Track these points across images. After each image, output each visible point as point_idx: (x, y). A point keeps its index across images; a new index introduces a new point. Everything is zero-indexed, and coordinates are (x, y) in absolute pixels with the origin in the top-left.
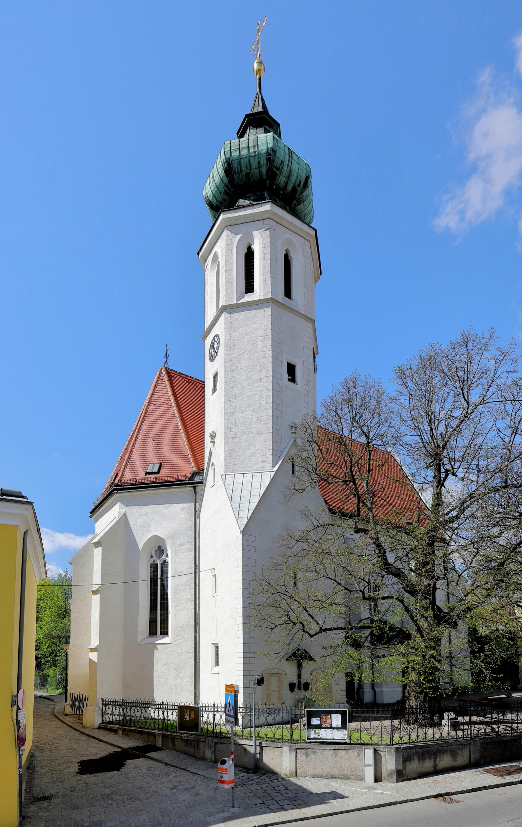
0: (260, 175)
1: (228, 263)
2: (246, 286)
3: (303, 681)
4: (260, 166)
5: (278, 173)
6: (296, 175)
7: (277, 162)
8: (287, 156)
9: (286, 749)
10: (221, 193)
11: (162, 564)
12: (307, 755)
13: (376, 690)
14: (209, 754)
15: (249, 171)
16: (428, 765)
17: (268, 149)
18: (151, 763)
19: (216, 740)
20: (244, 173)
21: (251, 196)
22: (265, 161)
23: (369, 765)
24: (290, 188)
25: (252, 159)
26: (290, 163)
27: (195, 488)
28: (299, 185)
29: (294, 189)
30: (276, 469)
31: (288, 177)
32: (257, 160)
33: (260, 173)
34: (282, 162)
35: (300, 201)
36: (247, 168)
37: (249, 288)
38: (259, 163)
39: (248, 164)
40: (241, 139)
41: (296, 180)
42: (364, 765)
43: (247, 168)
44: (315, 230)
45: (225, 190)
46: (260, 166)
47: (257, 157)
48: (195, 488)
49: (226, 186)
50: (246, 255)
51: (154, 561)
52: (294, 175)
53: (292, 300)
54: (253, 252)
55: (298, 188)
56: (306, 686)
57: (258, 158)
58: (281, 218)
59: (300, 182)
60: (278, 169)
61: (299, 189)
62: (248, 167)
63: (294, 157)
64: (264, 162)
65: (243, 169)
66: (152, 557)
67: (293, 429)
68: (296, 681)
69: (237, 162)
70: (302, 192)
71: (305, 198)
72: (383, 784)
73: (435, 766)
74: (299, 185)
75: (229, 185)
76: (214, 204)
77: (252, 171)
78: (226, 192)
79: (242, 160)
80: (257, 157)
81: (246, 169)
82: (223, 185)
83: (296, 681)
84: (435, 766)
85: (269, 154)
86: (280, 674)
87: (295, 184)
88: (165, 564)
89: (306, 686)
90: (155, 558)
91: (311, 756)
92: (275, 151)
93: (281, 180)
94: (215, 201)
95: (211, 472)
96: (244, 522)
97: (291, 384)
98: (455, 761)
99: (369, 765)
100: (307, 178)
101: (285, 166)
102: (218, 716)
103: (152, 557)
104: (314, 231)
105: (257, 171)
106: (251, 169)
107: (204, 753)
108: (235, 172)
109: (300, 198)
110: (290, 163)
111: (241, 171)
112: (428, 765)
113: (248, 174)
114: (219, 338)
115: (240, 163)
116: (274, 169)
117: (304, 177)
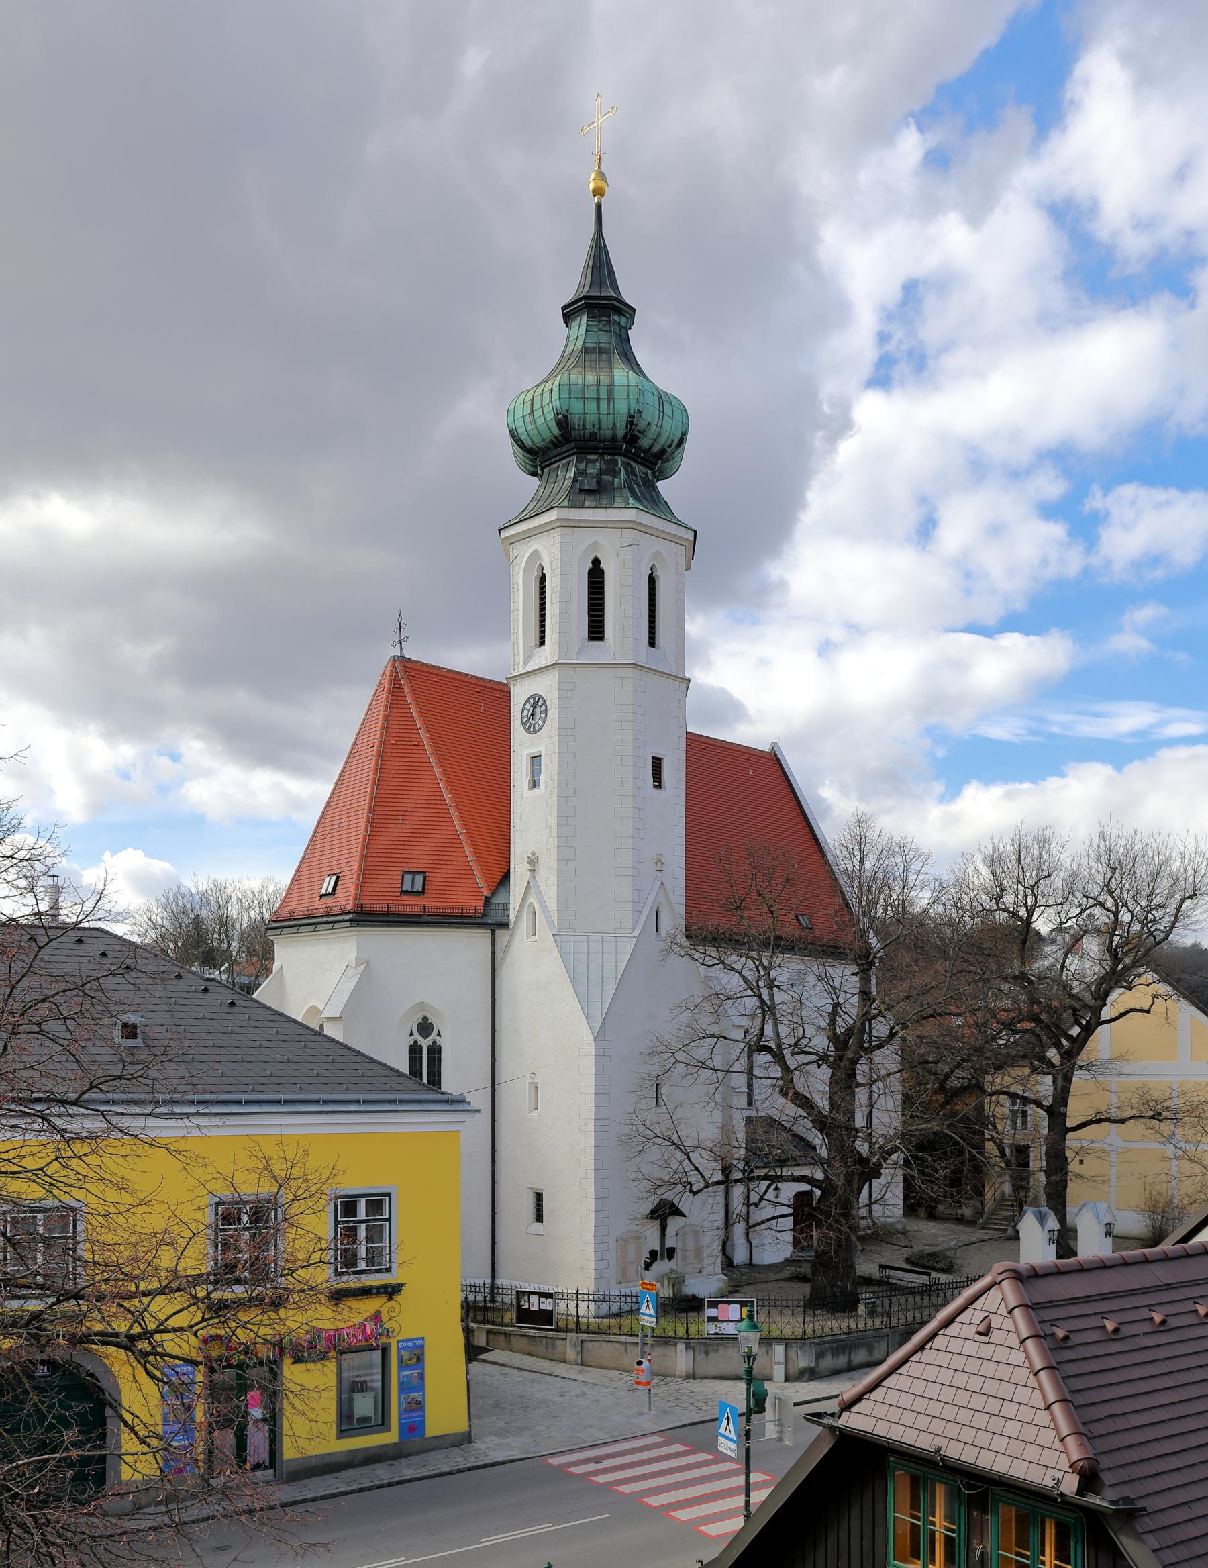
1: (564, 588)
3: (669, 1244)
4: (614, 427)
7: (642, 424)
9: (681, 1347)
10: (543, 440)
11: (429, 1048)
12: (707, 1354)
13: (753, 1242)
14: (571, 1354)
16: (842, 1361)
18: (488, 1368)
19: (583, 1336)
21: (594, 461)
22: (624, 424)
23: (779, 1363)
24: (656, 449)
27: (493, 932)
28: (670, 446)
30: (636, 934)
32: (611, 421)
37: (596, 631)
39: (596, 423)
42: (773, 1363)
46: (614, 427)
48: (493, 932)
50: (590, 572)
51: (416, 1042)
52: (665, 435)
56: (671, 1253)
66: (411, 1034)
68: (657, 1247)
73: (850, 1362)
83: (657, 1247)
84: (850, 1362)
86: (639, 1238)
88: (435, 1051)
89: (671, 1253)
90: (417, 1036)
91: (712, 1355)
92: (640, 412)
93: (645, 442)
96: (598, 1023)
97: (657, 791)
98: (871, 1355)
99: (779, 1363)
100: (684, 434)
101: (653, 427)
102: (583, 1305)
103: (411, 1034)
107: (565, 1353)
111: (584, 428)
112: (842, 1361)
117: (679, 435)
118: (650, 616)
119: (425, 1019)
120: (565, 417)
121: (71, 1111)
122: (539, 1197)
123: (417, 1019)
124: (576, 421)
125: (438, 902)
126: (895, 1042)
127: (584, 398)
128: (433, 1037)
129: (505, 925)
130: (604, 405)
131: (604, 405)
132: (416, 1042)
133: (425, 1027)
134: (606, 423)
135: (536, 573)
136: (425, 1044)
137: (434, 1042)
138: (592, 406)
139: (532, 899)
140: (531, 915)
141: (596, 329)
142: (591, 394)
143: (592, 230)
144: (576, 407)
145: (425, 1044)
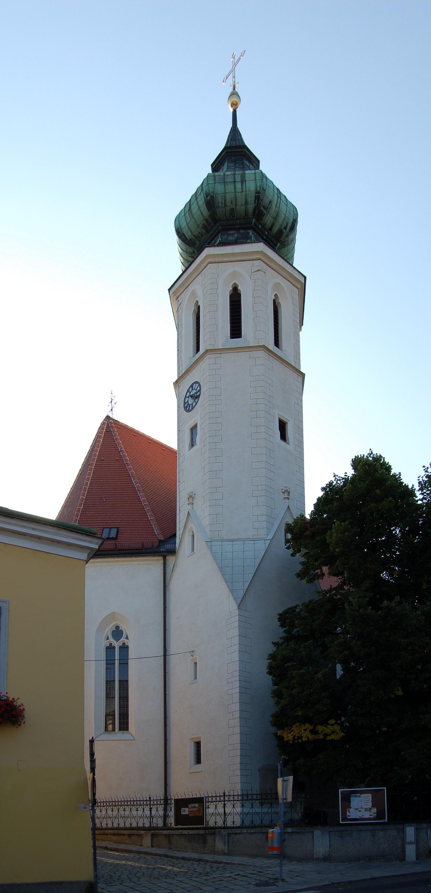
0: (246, 212)
2: (232, 330)
4: (246, 203)
5: (265, 212)
6: (283, 216)
7: (266, 202)
8: (276, 196)
10: (198, 227)
11: (120, 647)
15: (234, 207)
17: (256, 187)
20: (228, 209)
21: (233, 234)
22: (253, 199)
23: (410, 843)
24: (275, 229)
25: (238, 195)
26: (278, 204)
27: (165, 559)
28: (285, 228)
29: (280, 232)
31: (275, 218)
32: (244, 197)
33: (246, 211)
34: (270, 202)
35: (284, 245)
36: (232, 203)
38: (246, 200)
39: (234, 200)
40: (217, 174)
41: (283, 222)
43: (232, 203)
44: (305, 278)
45: (204, 225)
46: (246, 203)
47: (244, 193)
48: (165, 559)
49: (206, 220)
50: (231, 296)
51: (111, 644)
53: (282, 350)
54: (240, 295)
55: (284, 230)
57: (246, 195)
58: (272, 260)
59: (287, 224)
60: (266, 209)
61: (285, 232)
62: (234, 204)
63: (282, 198)
64: (251, 200)
65: (228, 204)
66: (108, 638)
67: (286, 494)
69: (222, 196)
70: (288, 236)
71: (289, 242)
72: (143, 844)
74: (285, 228)
75: (210, 220)
76: (188, 238)
77: (237, 207)
78: (204, 227)
79: (227, 194)
80: (244, 193)
81: (230, 204)
82: (202, 218)
85: (258, 192)
87: (281, 226)
88: (124, 648)
90: (111, 640)
93: (268, 220)
94: (190, 234)
95: (187, 539)
97: (283, 443)
99: (410, 843)
103: (108, 638)
104: (304, 278)
105: (243, 208)
106: (236, 205)
108: (219, 207)
109: (286, 241)
110: (278, 204)
111: (226, 206)
113: (232, 210)
114: (200, 385)
115: (225, 197)
116: (262, 208)
117: (292, 221)
118: (275, 335)
119: (117, 627)
120: (212, 197)
121: (243, 832)
122: (198, 745)
123: (110, 627)
124: (219, 200)
125: (124, 542)
126: (285, 831)
127: (224, 182)
128: (123, 639)
129: (173, 552)
130: (238, 186)
131: (238, 186)
132: (111, 644)
133: (117, 633)
134: (241, 200)
135: (193, 308)
136: (117, 645)
137: (124, 644)
138: (230, 187)
139: (191, 525)
140: (191, 538)
141: (233, 168)
142: (230, 179)
143: (230, 125)
144: (219, 189)
145: (117, 645)
